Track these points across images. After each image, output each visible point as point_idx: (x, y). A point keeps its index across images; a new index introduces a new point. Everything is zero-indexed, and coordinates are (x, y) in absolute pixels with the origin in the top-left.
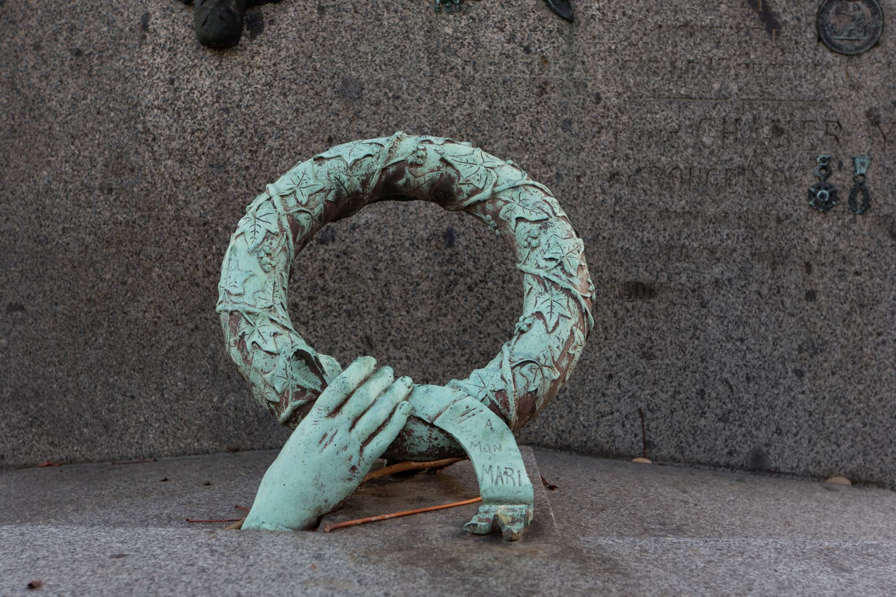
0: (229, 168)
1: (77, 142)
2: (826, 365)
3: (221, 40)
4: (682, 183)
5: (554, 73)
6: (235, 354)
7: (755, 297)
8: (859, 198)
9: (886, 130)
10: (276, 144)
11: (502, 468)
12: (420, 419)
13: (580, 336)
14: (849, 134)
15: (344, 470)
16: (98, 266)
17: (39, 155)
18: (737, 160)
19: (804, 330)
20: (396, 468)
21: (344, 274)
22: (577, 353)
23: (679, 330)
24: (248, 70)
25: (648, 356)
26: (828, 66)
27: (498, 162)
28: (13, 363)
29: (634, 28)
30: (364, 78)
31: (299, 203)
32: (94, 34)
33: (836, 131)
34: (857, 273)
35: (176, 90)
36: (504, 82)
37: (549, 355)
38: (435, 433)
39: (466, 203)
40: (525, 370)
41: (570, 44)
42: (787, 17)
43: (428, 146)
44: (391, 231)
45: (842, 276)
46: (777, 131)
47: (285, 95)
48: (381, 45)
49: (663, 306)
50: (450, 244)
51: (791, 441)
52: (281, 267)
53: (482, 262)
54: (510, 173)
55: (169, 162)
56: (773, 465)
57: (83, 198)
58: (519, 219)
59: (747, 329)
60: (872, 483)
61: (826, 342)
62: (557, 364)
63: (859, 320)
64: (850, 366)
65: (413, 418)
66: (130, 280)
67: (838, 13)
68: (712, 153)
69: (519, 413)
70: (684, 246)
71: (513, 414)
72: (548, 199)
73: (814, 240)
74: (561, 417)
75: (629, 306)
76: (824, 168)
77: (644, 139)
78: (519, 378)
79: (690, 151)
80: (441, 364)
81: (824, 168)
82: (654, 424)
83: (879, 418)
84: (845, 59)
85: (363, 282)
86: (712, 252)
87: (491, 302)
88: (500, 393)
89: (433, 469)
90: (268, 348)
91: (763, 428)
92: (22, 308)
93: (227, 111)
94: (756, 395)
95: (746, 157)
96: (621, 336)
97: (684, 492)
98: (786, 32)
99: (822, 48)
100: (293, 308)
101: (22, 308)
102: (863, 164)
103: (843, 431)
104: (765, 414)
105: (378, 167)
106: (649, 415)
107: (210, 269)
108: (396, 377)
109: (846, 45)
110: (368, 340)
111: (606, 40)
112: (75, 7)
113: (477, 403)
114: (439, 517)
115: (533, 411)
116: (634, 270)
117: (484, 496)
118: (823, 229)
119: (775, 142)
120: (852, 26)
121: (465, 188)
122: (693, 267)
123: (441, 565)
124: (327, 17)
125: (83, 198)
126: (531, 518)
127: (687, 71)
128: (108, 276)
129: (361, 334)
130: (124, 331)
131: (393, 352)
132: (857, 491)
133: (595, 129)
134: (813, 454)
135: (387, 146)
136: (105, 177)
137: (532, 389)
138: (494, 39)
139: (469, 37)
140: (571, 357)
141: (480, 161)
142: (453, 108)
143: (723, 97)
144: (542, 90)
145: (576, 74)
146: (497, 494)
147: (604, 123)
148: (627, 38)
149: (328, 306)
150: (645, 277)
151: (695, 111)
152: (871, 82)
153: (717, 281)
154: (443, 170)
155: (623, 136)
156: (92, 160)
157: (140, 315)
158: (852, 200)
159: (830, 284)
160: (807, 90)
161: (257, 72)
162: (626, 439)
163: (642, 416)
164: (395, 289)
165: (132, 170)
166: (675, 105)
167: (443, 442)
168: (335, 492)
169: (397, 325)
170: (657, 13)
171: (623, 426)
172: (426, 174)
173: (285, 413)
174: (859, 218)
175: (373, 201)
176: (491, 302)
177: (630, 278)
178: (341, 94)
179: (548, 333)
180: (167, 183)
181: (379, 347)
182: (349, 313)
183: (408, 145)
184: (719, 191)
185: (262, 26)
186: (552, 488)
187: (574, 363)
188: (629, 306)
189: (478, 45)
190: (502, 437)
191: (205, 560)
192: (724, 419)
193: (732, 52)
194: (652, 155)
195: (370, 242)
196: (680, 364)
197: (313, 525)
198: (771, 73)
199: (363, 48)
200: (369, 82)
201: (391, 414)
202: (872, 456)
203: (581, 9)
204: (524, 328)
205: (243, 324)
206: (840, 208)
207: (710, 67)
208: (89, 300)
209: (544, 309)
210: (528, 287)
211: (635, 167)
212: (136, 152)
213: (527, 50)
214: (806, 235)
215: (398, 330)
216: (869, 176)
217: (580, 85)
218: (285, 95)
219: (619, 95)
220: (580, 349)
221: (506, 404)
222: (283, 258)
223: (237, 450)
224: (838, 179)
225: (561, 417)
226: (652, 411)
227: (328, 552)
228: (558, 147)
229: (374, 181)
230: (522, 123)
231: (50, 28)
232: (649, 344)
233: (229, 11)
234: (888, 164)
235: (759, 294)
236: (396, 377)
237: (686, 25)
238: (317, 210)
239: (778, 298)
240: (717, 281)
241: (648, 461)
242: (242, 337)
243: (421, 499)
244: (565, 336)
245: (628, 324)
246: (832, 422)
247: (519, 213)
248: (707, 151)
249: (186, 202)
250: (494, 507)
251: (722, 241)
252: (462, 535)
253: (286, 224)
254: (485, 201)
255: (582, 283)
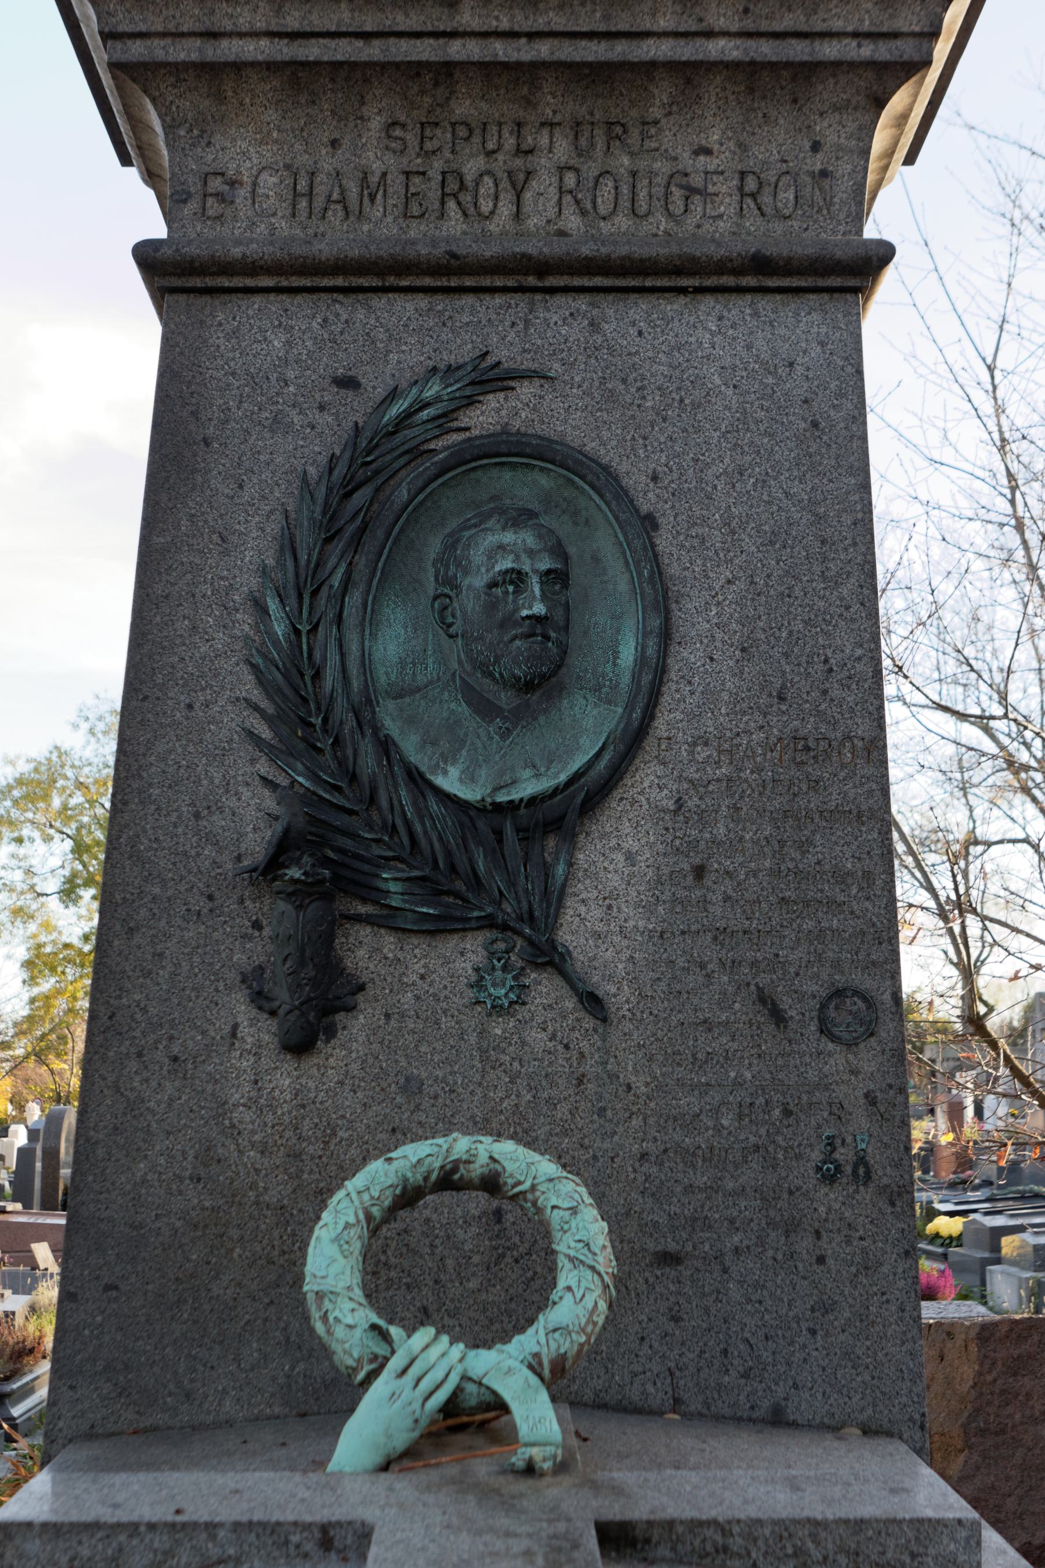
0: (304, 1157)
1: (172, 1138)
2: (836, 1323)
3: (300, 1045)
4: (704, 1161)
5: (590, 1067)
6: (319, 1328)
7: (770, 1262)
8: (861, 1171)
9: (882, 1110)
10: (346, 1135)
11: (537, 1420)
12: (470, 1379)
13: (603, 1306)
14: (850, 1114)
15: (409, 1422)
16: (186, 1248)
17: (138, 1149)
18: (752, 1139)
19: (815, 1291)
20: (451, 1422)
21: (404, 1250)
22: (601, 1320)
23: (704, 1295)
24: (322, 1070)
25: (676, 1319)
26: (830, 1054)
27: (537, 1157)
28: (107, 1338)
29: (660, 1025)
30: (424, 1075)
31: (372, 1198)
32: (190, 1042)
33: (839, 1112)
34: (861, 1239)
35: (259, 1090)
36: (547, 1075)
37: (576, 1322)
38: (483, 1390)
39: (511, 1193)
40: (557, 1335)
41: (604, 1041)
42: (793, 1013)
43: (479, 1146)
44: (446, 1211)
45: (848, 1242)
46: (787, 1113)
47: (355, 1092)
48: (439, 1045)
49: (689, 1273)
50: (499, 1221)
51: (807, 1395)
52: (357, 1252)
53: (528, 1236)
54: (547, 1167)
55: (252, 1153)
56: (791, 1418)
57: (174, 1187)
58: (554, 1207)
59: (765, 1292)
60: (882, 1433)
61: (836, 1303)
62: (583, 1330)
63: (865, 1281)
64: (858, 1324)
65: (465, 1378)
66: (214, 1260)
67: (837, 1008)
68: (730, 1133)
69: (552, 1371)
70: (706, 1217)
71: (546, 1372)
72: (579, 1189)
73: (822, 1209)
74: (599, 1377)
75: (659, 1273)
76: (829, 1144)
77: (670, 1122)
78: (551, 1342)
79: (711, 1132)
80: (489, 1329)
81: (829, 1144)
82: (682, 1382)
83: (886, 1371)
84: (844, 1048)
85: (421, 1257)
86: (732, 1222)
87: (535, 1273)
88: (537, 1355)
89: (483, 1424)
90: (345, 1319)
91: (781, 1383)
92: (116, 1288)
93: (303, 1106)
94: (774, 1353)
95: (760, 1137)
96: (652, 1301)
97: (704, 1442)
98: (792, 1025)
99: (824, 1039)
100: (364, 1286)
101: (116, 1288)
102: (863, 1140)
103: (854, 1384)
104: (782, 1370)
105: (437, 1165)
106: (678, 1373)
107: (285, 1248)
108: (451, 1344)
109: (845, 1036)
110: (425, 1310)
111: (635, 1037)
112: (174, 1020)
113: (517, 1364)
114: (485, 1460)
115: (563, 1370)
116: (662, 1240)
117: (522, 1440)
118: (829, 1199)
119: (785, 1122)
120: (850, 1019)
121: (510, 1181)
122: (715, 1236)
123: (486, 1493)
124: (392, 1022)
125: (174, 1187)
126: (559, 1458)
127: (706, 1062)
128: (194, 1257)
129: (418, 1304)
130: (207, 1307)
131: (447, 1321)
132: (865, 1440)
133: (627, 1115)
134: (827, 1407)
135: (445, 1147)
136: (194, 1168)
137: (562, 1351)
138: (537, 1038)
139: (515, 1037)
140: (595, 1324)
141: (522, 1157)
142: (502, 1100)
143: (738, 1083)
144: (580, 1081)
145: (609, 1067)
146: (532, 1439)
147: (635, 1109)
148: (654, 1035)
149: (389, 1280)
150: (672, 1246)
151: (715, 1097)
152: (868, 1067)
153: (737, 1249)
154: (492, 1166)
155: (651, 1121)
156: (184, 1153)
157: (222, 1292)
158: (855, 1173)
159: (837, 1249)
160: (812, 1075)
161: (330, 1072)
162: (657, 1395)
163: (671, 1374)
164: (450, 1263)
165: (219, 1161)
166: (696, 1092)
167: (489, 1398)
168: (401, 1440)
169: (451, 1296)
170: (680, 1012)
171: (655, 1383)
172: (477, 1170)
173: (361, 1376)
174: (862, 1188)
175: (431, 1192)
176: (535, 1273)
177: (659, 1248)
178: (404, 1089)
179: (577, 1303)
180: (249, 1173)
181: (435, 1316)
182: (408, 1286)
183: (461, 1144)
184: (736, 1168)
185: (336, 1032)
186: (585, 1440)
187: (597, 1329)
188: (659, 1273)
189: (524, 1043)
190: (537, 1391)
191: (303, 1493)
192: (746, 1375)
193: (745, 1044)
194: (677, 1136)
195: (428, 1220)
196: (705, 1325)
197: (385, 1467)
198: (780, 1062)
199: (423, 1049)
200: (428, 1078)
201: (447, 1375)
202: (881, 1407)
203: (614, 1010)
204: (557, 1299)
205: (326, 1302)
206: (844, 1180)
207: (726, 1058)
208: (177, 1279)
209: (573, 1284)
210: (560, 1265)
211: (663, 1148)
212: (223, 1145)
213: (567, 1047)
214: (815, 1205)
215: (452, 1300)
216: (870, 1150)
217: (613, 1077)
218: (355, 1092)
219: (647, 1084)
220: (603, 1317)
221: (540, 1364)
222: (358, 1245)
223: (304, 1415)
224: (842, 1154)
225: (599, 1377)
226: (680, 1370)
227: (398, 1486)
228: (594, 1131)
229: (434, 1177)
230: (562, 1111)
231: (151, 1038)
232: (676, 1308)
233: (308, 1022)
234: (885, 1139)
235: (775, 1259)
236: (451, 1344)
237: (705, 1022)
238: (387, 1203)
239: (791, 1263)
240: (737, 1249)
241: (677, 1417)
242: (327, 1312)
243: (471, 1448)
244: (590, 1306)
245: (657, 1289)
246: (844, 1377)
247: (554, 1201)
248: (725, 1132)
249: (266, 1189)
250: (529, 1449)
251: (740, 1212)
252: (504, 1472)
253: (361, 1216)
254: (525, 1192)
255: (605, 1261)
